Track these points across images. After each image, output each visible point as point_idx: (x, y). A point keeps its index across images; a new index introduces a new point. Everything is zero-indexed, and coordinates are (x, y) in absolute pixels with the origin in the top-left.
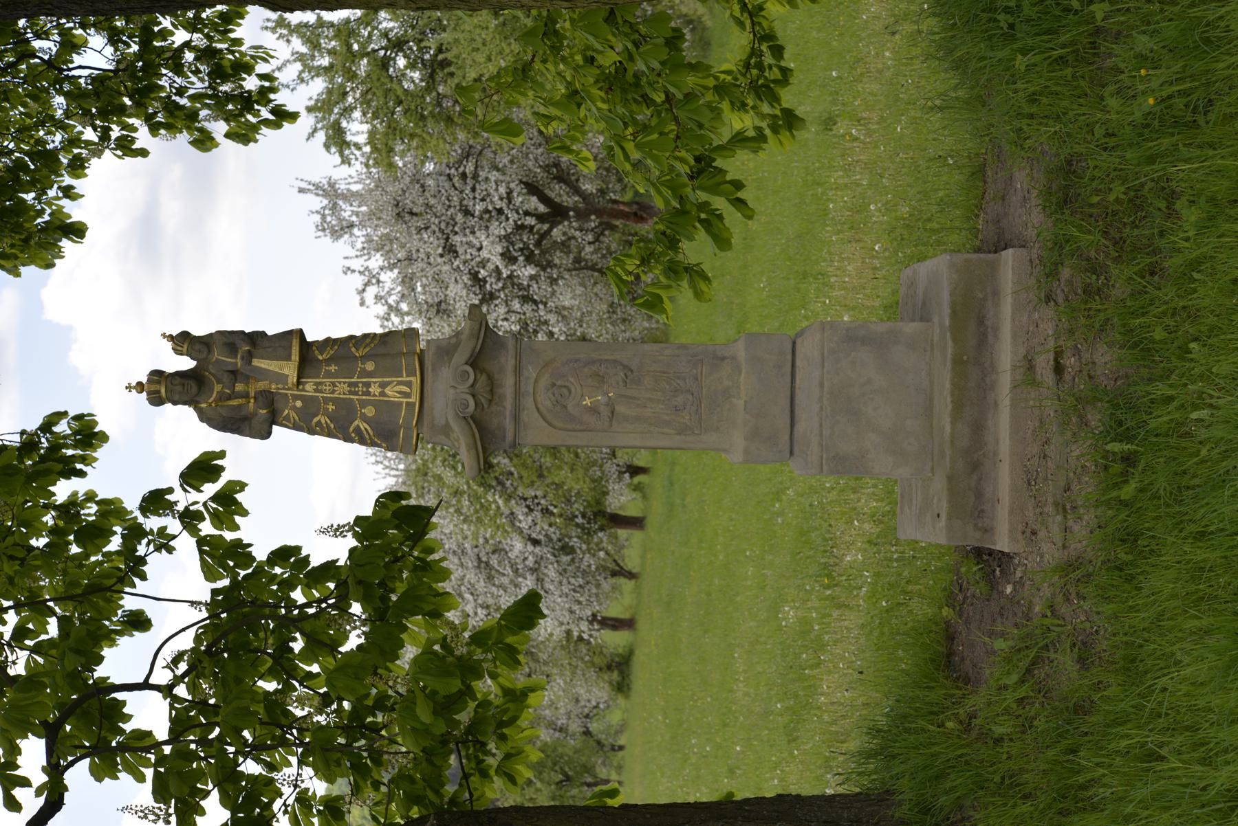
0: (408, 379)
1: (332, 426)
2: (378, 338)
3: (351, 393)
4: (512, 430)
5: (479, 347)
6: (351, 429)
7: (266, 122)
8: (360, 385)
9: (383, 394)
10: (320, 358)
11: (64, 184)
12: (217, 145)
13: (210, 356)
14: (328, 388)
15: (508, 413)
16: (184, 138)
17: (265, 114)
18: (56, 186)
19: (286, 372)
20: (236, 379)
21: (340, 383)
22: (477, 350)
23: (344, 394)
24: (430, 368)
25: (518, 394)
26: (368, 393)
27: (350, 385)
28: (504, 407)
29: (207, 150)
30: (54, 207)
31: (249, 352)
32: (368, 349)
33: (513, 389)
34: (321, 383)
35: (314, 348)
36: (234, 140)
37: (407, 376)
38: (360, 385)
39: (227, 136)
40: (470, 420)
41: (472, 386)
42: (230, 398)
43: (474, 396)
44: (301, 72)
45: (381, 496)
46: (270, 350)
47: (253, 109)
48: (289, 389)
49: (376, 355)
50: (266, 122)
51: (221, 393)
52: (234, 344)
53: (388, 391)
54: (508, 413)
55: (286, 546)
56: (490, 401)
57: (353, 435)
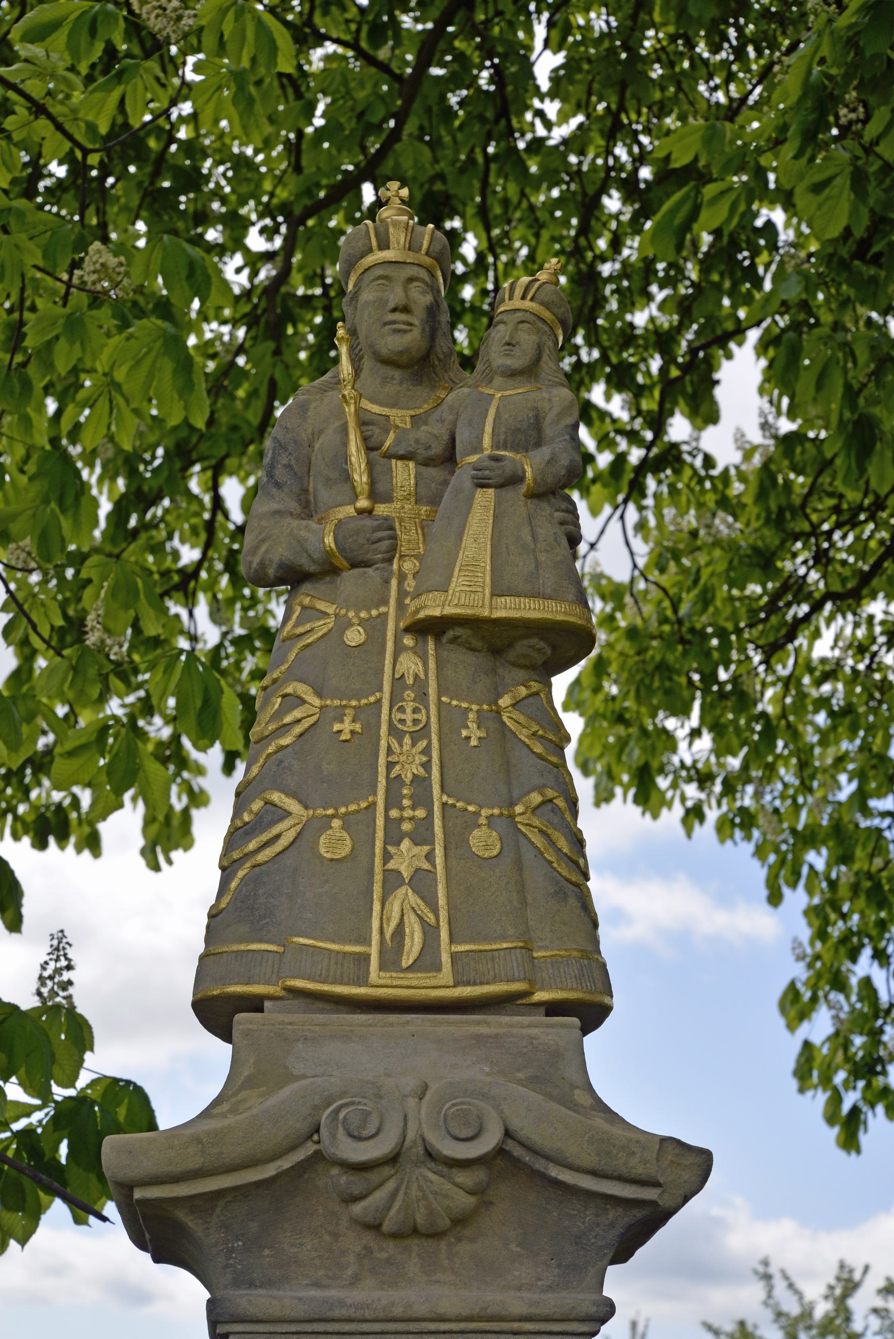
0: (445, 958)
1: (286, 741)
2: (575, 877)
3: (394, 783)
4: (274, 1309)
5: (567, 1176)
6: (276, 797)
7: (836, 1099)
8: (420, 813)
9: (393, 880)
10: (505, 701)
11: (706, 809)
12: (791, 1027)
13: (498, 380)
14: (409, 716)
15: (333, 1293)
16: (800, 972)
17: (850, 1099)
18: (703, 796)
19: (458, 582)
20: (427, 462)
21: (427, 751)
22: (555, 1172)
23: (390, 766)
24: (484, 1030)
25: (408, 987)
26: (393, 837)
27: (421, 783)
28: (355, 1281)
29: (783, 1008)
30: (669, 794)
31: (516, 479)
32: (538, 841)
33: (421, 1309)
34: (422, 697)
35: (535, 686)
36: (801, 1055)
37: (454, 956)
38: (420, 813)
39: (807, 1045)
40: (310, 1149)
41: (430, 1154)
42: (370, 446)
43: (393, 1159)
44: (787, 1315)
45: (135, 1084)
46: (527, 537)
47: (856, 1079)
48: (401, 606)
49: (519, 865)
50: (836, 1099)
51: (385, 424)
52: (538, 444)
53: (406, 896)
54: (333, 1293)
55: (89, 1027)
56: (375, 1227)
57: (257, 805)
